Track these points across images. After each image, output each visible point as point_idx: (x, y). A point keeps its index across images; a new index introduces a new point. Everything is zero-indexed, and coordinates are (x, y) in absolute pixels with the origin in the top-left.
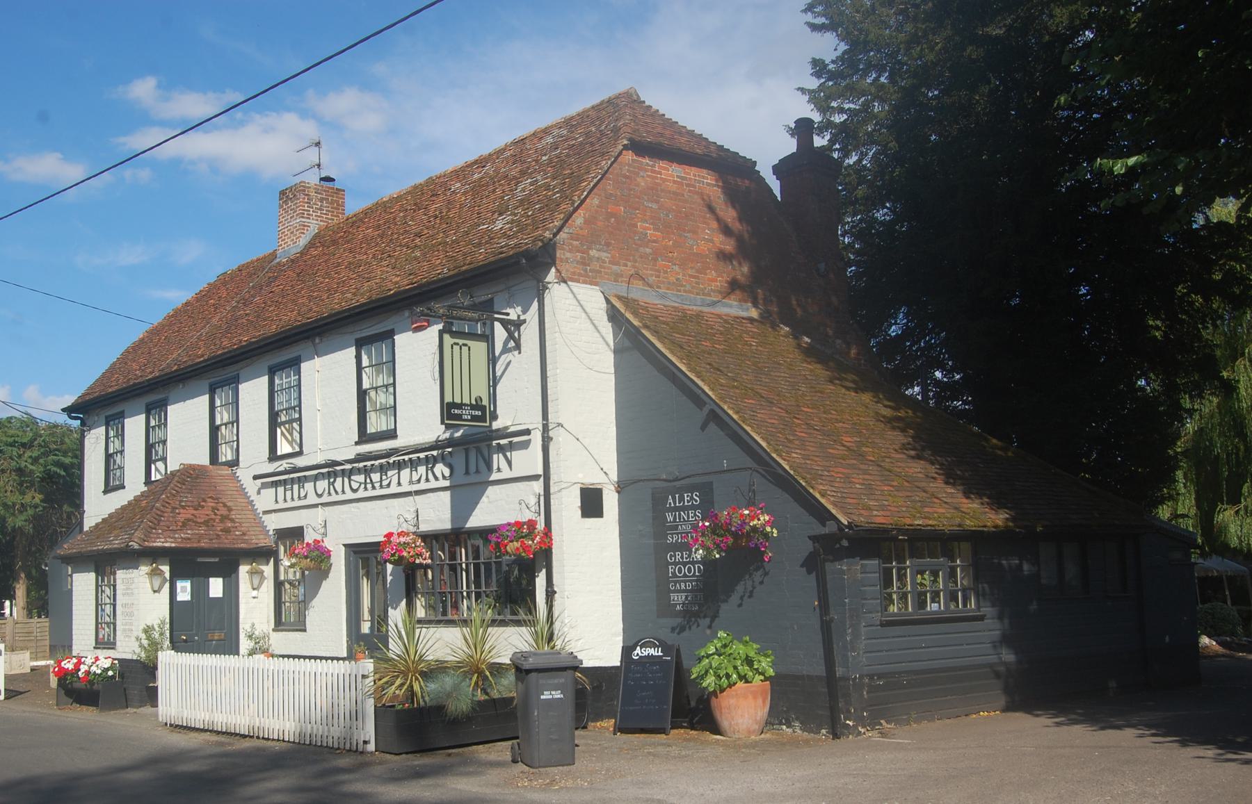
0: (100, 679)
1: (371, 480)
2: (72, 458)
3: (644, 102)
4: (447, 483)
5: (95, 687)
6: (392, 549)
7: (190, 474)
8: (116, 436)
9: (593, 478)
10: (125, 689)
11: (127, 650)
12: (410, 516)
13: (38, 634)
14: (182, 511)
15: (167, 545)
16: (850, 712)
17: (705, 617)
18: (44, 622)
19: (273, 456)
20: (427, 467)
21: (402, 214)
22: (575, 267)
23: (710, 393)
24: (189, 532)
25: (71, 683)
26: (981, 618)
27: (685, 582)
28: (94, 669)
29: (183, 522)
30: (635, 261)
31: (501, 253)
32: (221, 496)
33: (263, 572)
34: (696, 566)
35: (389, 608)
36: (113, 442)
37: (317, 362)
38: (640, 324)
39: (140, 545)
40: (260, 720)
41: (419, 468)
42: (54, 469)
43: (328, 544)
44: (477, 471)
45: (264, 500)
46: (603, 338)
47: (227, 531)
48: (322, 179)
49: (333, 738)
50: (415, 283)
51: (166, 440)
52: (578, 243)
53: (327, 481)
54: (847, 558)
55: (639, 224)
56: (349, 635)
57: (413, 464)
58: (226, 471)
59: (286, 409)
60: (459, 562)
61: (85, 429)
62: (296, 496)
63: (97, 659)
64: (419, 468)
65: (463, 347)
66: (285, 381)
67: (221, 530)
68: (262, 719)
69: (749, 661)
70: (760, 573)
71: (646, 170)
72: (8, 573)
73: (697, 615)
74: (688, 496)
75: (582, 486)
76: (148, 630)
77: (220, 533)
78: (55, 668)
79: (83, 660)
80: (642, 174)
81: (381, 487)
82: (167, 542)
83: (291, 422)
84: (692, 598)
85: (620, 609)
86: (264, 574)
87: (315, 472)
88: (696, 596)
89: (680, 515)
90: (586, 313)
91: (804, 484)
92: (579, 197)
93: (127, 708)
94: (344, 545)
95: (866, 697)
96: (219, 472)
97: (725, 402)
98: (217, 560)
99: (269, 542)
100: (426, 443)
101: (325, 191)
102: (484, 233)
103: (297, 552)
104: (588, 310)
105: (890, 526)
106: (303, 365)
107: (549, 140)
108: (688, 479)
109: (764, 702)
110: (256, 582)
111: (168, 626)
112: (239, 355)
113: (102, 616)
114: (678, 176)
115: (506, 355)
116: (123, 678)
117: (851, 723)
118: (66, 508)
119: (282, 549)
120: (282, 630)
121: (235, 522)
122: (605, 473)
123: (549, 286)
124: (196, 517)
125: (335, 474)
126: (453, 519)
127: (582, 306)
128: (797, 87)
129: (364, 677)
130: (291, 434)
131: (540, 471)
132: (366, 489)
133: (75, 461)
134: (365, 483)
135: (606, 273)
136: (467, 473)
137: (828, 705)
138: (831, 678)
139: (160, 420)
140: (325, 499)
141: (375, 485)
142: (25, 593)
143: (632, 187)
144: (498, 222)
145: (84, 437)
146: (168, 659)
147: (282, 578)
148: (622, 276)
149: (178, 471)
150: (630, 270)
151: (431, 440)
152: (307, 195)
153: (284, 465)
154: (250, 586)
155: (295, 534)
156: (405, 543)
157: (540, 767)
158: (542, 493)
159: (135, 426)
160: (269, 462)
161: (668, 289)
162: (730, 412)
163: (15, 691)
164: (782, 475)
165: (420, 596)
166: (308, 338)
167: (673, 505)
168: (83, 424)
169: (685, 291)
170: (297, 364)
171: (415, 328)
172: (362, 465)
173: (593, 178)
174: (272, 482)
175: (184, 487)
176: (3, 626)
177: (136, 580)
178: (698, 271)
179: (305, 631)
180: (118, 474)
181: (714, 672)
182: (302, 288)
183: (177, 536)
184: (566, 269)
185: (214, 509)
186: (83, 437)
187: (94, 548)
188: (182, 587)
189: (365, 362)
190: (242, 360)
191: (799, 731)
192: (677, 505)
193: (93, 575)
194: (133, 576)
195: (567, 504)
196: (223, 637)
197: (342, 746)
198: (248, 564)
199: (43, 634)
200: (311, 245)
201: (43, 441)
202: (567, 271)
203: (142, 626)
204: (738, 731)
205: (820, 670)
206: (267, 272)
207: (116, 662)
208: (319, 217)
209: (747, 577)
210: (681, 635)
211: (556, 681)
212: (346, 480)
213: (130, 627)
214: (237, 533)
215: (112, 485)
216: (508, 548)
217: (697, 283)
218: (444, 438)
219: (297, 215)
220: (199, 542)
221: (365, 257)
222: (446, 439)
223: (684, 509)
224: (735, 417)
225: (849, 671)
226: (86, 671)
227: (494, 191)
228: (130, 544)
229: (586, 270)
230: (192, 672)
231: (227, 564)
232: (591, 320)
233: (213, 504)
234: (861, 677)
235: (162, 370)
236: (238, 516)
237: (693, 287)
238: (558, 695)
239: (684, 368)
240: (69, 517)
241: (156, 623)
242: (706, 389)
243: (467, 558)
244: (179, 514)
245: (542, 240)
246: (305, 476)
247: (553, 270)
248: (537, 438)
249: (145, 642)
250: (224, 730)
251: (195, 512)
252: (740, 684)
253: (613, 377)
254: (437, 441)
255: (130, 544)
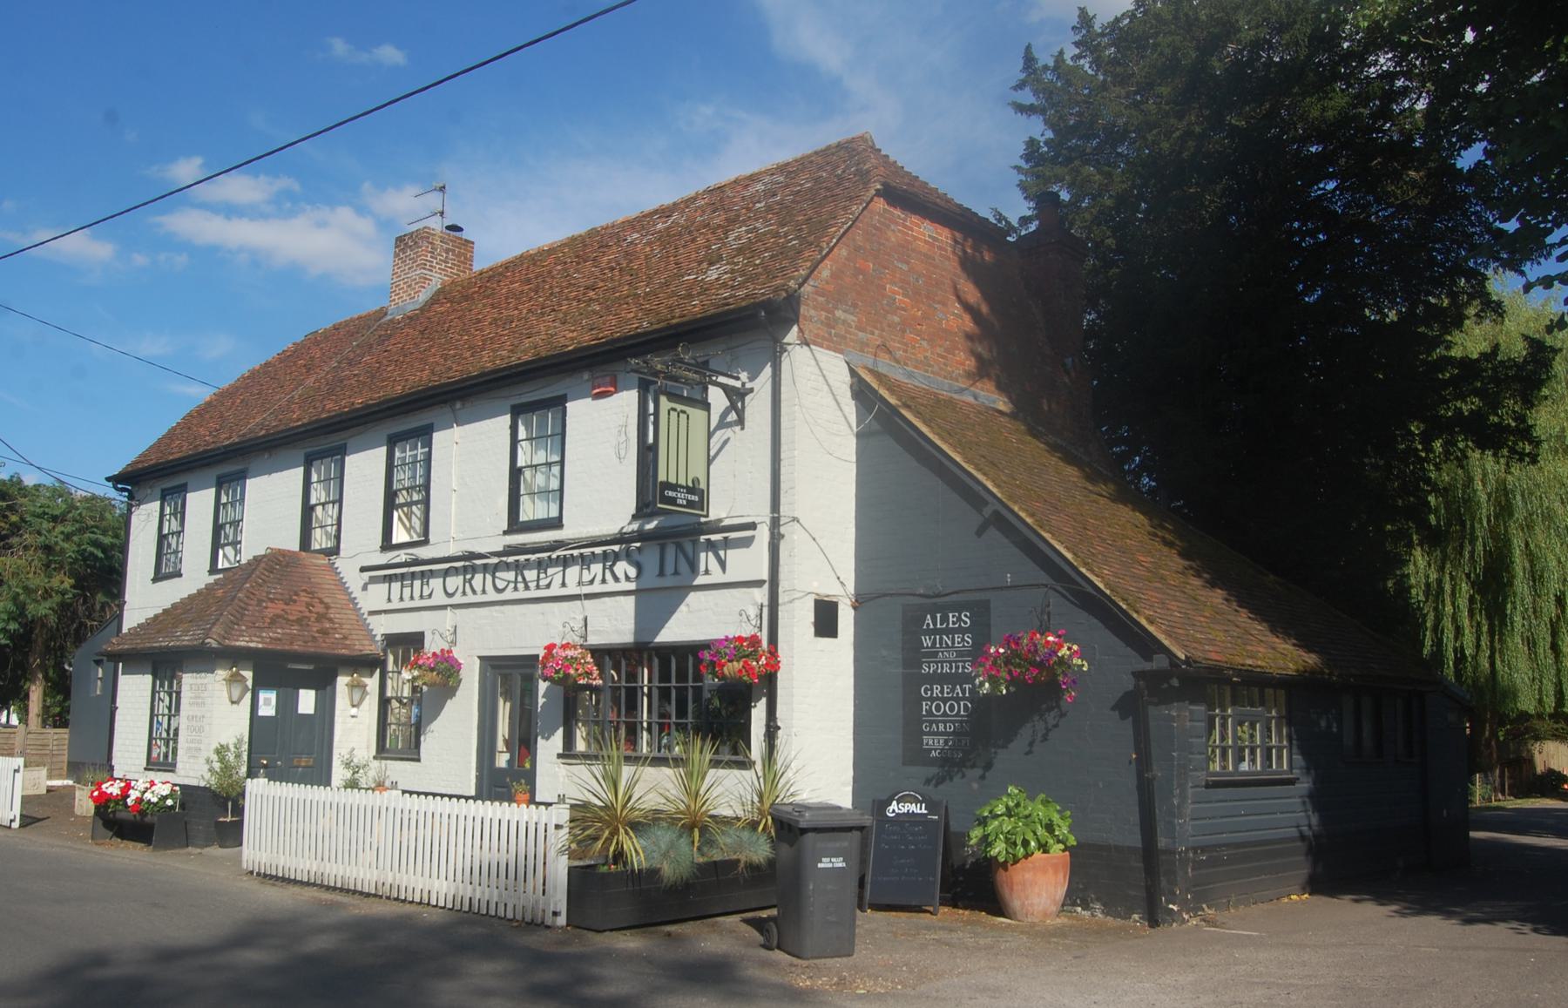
0: (156, 809)
1: (524, 578)
2: (113, 538)
3: (880, 150)
4: (632, 586)
5: (148, 819)
6: (558, 664)
7: (275, 562)
8: (175, 514)
9: (831, 590)
10: (186, 823)
11: (191, 774)
12: (578, 625)
13: (55, 748)
14: (269, 604)
15: (252, 645)
16: (1175, 894)
17: (973, 766)
18: (63, 734)
19: (387, 544)
20: (465, 579)
21: (559, 267)
22: (819, 328)
23: (995, 490)
24: (279, 631)
25: (114, 812)
26: (1291, 782)
27: (945, 722)
28: (148, 796)
29: (271, 619)
30: (883, 330)
31: (728, 304)
32: (316, 590)
33: (365, 686)
34: (962, 703)
35: (539, 738)
36: (169, 521)
37: (457, 431)
38: (899, 403)
39: (219, 643)
40: (395, 874)
41: (592, 566)
42: (91, 549)
43: (457, 653)
44: (676, 573)
45: (373, 598)
46: (846, 418)
47: (324, 632)
48: (449, 228)
49: (506, 905)
50: (602, 338)
51: (242, 520)
52: (823, 299)
53: (461, 577)
54: (1177, 701)
55: (888, 286)
56: (480, 768)
57: (585, 561)
58: (323, 561)
59: (407, 489)
60: (640, 684)
61: (133, 503)
62: (417, 594)
63: (152, 783)
64: (592, 566)
65: (681, 415)
66: (408, 453)
67: (318, 632)
68: (397, 874)
69: (1050, 828)
70: (1053, 714)
71: (897, 224)
72: (19, 672)
73: (962, 764)
74: (953, 617)
75: (817, 597)
76: (221, 751)
77: (317, 635)
78: (93, 792)
79: (133, 783)
80: (893, 227)
81: (538, 587)
82: (252, 641)
83: (409, 504)
84: (954, 742)
85: (851, 753)
86: (367, 688)
87: (446, 566)
88: (960, 741)
89: (941, 639)
90: (829, 385)
91: (1124, 607)
92: (828, 244)
93: (188, 846)
94: (479, 657)
95: (1190, 874)
96: (314, 561)
97: (1015, 502)
98: (311, 667)
99: (375, 649)
100: (609, 535)
101: (452, 241)
102: (693, 284)
103: (421, 662)
104: (831, 381)
105: (1225, 665)
106: (435, 435)
107: (760, 187)
108: (955, 596)
109: (1065, 877)
110: (357, 697)
111: (246, 747)
112: (351, 419)
113: (158, 729)
114: (930, 236)
115: (723, 431)
116: (184, 809)
117: (1175, 908)
118: (100, 597)
119: (391, 658)
120: (386, 759)
121: (334, 623)
122: (842, 583)
123: (789, 348)
124: (286, 613)
125: (474, 570)
126: (637, 631)
127: (824, 376)
128: (1013, 165)
129: (558, 827)
130: (410, 520)
131: (765, 575)
132: (516, 589)
133: (115, 541)
134: (516, 582)
135: (852, 340)
136: (661, 573)
137: (1143, 884)
138: (1150, 853)
139: (234, 495)
140: (458, 599)
141: (530, 584)
142: (41, 697)
143: (882, 241)
144: (709, 272)
145: (131, 513)
146: (258, 789)
147: (389, 694)
148: (867, 345)
149: (264, 556)
150: (876, 340)
151: (611, 532)
152: (431, 243)
153: (402, 556)
154: (349, 703)
155: (409, 643)
156: (572, 658)
157: (813, 958)
158: (766, 603)
159: (201, 503)
160: (381, 552)
161: (916, 367)
162: (1023, 515)
163: (30, 817)
164: (1089, 594)
165: (580, 724)
166: (445, 402)
167: (932, 626)
168: (131, 497)
169: (932, 372)
170: (427, 434)
171: (596, 394)
172: (511, 560)
173: (844, 223)
174: (385, 576)
175: (272, 576)
176: (12, 736)
177: (210, 687)
178: (947, 350)
179: (418, 760)
180: (173, 559)
181: (1006, 838)
182: (431, 346)
183: (264, 634)
184: (811, 329)
185: (308, 605)
186: (130, 512)
187: (155, 645)
188: (265, 699)
189: (522, 433)
190: (353, 427)
191: (1100, 915)
192: (939, 626)
193: (148, 678)
194: (206, 681)
195: (798, 620)
196: (311, 763)
197: (519, 917)
198: (347, 675)
199: (61, 747)
200: (434, 300)
201: (80, 514)
202: (810, 331)
203: (215, 745)
204: (1033, 914)
205: (1135, 840)
206: (375, 330)
207: (177, 788)
208: (444, 270)
209: (1036, 718)
210: (941, 787)
211: (838, 845)
212: (488, 577)
213: (199, 746)
214: (337, 636)
215: (164, 571)
216: (725, 669)
217: (945, 364)
218: (630, 530)
219: (417, 266)
220: (291, 644)
221: (516, 312)
222: (633, 532)
223: (948, 631)
224: (1029, 520)
225: (1175, 842)
226: (137, 798)
227: (693, 240)
228: (207, 641)
229: (830, 334)
230: (295, 808)
231: (322, 674)
232: (833, 394)
233: (306, 599)
234: (1187, 850)
235: (244, 435)
236: (337, 616)
237: (941, 369)
238: (839, 863)
239: (958, 459)
240: (103, 608)
241: (231, 742)
242: (989, 485)
243: (650, 680)
244: (266, 608)
245: (786, 291)
246: (431, 571)
247: (795, 328)
248: (763, 535)
249: (217, 766)
250: (339, 885)
251: (285, 607)
252: (1038, 854)
253: (854, 466)
254: (620, 532)
255: (207, 641)
